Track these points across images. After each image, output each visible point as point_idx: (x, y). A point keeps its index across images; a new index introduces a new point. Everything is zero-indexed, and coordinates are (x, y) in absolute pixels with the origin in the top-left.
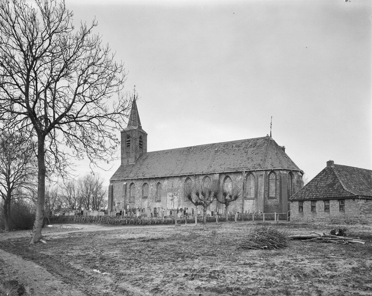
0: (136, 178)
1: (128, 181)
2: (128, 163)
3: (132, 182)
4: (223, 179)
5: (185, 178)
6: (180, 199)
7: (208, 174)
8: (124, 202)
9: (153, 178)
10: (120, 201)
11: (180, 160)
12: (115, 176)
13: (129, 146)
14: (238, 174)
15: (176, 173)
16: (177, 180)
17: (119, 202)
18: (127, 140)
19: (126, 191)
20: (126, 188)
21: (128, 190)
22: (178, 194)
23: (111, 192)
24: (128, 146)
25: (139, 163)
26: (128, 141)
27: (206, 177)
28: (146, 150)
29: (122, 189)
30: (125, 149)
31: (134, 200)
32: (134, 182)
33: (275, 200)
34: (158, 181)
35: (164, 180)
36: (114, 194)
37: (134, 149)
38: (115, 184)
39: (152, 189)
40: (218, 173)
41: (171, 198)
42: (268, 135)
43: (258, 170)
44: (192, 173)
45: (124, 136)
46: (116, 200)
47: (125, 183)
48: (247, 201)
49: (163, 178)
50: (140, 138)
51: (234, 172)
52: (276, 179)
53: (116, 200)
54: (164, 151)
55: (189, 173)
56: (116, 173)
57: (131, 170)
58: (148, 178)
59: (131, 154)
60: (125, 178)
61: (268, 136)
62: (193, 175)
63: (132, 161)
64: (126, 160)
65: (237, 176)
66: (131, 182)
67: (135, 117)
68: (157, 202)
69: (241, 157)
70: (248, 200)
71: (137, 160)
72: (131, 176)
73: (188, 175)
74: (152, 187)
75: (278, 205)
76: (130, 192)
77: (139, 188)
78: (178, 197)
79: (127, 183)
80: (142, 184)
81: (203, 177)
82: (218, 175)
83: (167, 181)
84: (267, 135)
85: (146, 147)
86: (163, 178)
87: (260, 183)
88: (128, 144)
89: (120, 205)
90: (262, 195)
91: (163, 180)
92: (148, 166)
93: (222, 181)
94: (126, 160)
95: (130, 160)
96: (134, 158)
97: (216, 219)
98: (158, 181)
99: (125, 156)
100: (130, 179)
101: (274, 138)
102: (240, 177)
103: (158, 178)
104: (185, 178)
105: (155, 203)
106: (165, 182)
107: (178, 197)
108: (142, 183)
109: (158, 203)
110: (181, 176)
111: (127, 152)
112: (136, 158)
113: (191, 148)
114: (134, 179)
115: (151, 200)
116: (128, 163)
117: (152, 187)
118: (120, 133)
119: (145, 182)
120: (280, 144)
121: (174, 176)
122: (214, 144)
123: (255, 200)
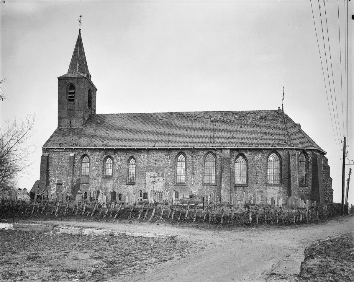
0: (94, 148)
1: (78, 151)
2: (71, 126)
3: (84, 153)
4: (234, 157)
5: (176, 153)
6: (168, 182)
7: (214, 149)
8: (71, 183)
9: (122, 150)
10: (62, 181)
11: (160, 128)
12: (51, 142)
13: (73, 100)
14: (256, 152)
15: (161, 144)
16: (162, 154)
17: (60, 182)
18: (69, 92)
19: (74, 166)
20: (74, 162)
21: (77, 165)
22: (165, 175)
23: (45, 166)
24: (70, 100)
25: (91, 127)
26: (70, 93)
27: (209, 154)
28: (95, 111)
29: (65, 161)
30: (65, 105)
31: (88, 181)
32: (88, 153)
33: (307, 187)
34: (131, 155)
35: (141, 153)
36: (51, 170)
37: (81, 105)
38: (53, 155)
39: (120, 165)
40: (228, 149)
41: (153, 179)
42: (279, 108)
43: (286, 149)
44: (187, 146)
45: (64, 84)
46: (54, 179)
47: (72, 154)
48: (271, 187)
49: (139, 150)
50: (90, 91)
51: (253, 149)
52: (307, 162)
53: (54, 179)
54: (129, 114)
55: (183, 146)
56: (51, 137)
57: (79, 136)
58: (115, 148)
59: (77, 113)
60: (72, 146)
61: (279, 110)
62: (191, 149)
63: (77, 123)
64: (67, 121)
65: (255, 154)
66: (82, 153)
67: (79, 56)
68: (129, 185)
69: (253, 131)
70: (272, 186)
71: (86, 123)
72: (82, 144)
73: (182, 149)
74: (119, 163)
75: (310, 195)
76: (80, 168)
77: (97, 163)
78: (164, 178)
79: (75, 154)
80: (103, 158)
81: (205, 152)
82: (228, 151)
83: (146, 155)
84: (278, 108)
85: (95, 107)
86: (139, 150)
87: (293, 165)
88: (70, 97)
89: (62, 187)
90: (296, 180)
91: (139, 154)
92: (108, 132)
93: (232, 160)
94: (67, 121)
95: (74, 121)
96: (82, 119)
97: (183, 208)
98: (131, 155)
99: (65, 114)
100: (83, 148)
101: (286, 112)
102: (260, 156)
103: (131, 149)
104: (176, 153)
105: (126, 186)
106: (142, 157)
107: (164, 178)
108: (103, 155)
109: (131, 186)
110: (171, 150)
111: (69, 109)
112: (84, 120)
113: (172, 114)
114: (89, 149)
115: (119, 182)
116: (71, 126)
117: (119, 163)
118: (57, 80)
119: (108, 154)
120: (297, 122)
121: (159, 149)
122: (206, 112)
123: (281, 188)
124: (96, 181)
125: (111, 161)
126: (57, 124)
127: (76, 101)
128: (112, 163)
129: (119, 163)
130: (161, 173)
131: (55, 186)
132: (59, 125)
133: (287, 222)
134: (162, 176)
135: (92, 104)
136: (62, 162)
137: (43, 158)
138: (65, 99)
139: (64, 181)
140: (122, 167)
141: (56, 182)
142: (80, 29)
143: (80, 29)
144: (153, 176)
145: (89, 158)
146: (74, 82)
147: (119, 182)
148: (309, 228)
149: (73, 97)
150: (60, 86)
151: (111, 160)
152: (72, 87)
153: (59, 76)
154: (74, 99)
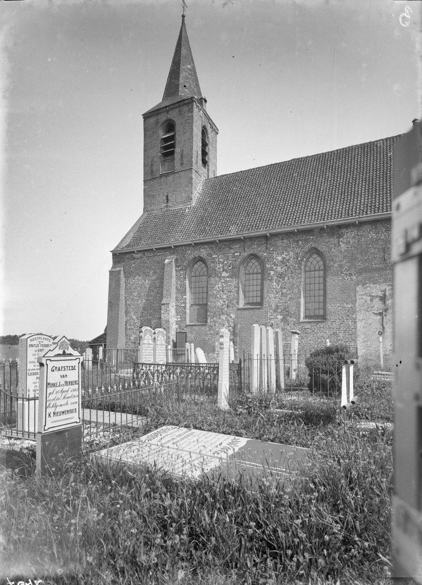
13: (172, 153)
115: (280, 317)
124: (223, 317)
125: (259, 267)
126: (143, 206)
127: (177, 156)
129: (279, 269)
132: (145, 209)
133: (161, 279)
135: (209, 159)
137: (111, 273)
138: (157, 152)
142: (183, 16)
143: (183, 16)
145: (207, 266)
151: (256, 264)
152: (170, 126)
153: (144, 112)
154: (174, 151)
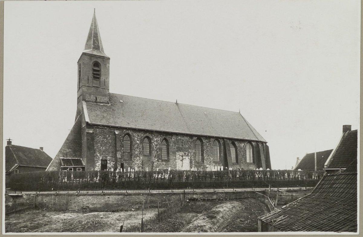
10: (106, 157)
13: (99, 78)
22: (189, 155)
35: (172, 136)
53: (99, 155)
78: (189, 157)
124: (138, 158)
128: (148, 142)
130: (187, 153)
131: (100, 162)
134: (188, 155)
136: (107, 139)
139: (109, 157)
140: (158, 147)
141: (101, 158)
144: (182, 155)
146: (99, 61)
147: (156, 159)
148: (339, 141)
149: (98, 75)
150: (312, 153)
